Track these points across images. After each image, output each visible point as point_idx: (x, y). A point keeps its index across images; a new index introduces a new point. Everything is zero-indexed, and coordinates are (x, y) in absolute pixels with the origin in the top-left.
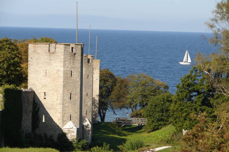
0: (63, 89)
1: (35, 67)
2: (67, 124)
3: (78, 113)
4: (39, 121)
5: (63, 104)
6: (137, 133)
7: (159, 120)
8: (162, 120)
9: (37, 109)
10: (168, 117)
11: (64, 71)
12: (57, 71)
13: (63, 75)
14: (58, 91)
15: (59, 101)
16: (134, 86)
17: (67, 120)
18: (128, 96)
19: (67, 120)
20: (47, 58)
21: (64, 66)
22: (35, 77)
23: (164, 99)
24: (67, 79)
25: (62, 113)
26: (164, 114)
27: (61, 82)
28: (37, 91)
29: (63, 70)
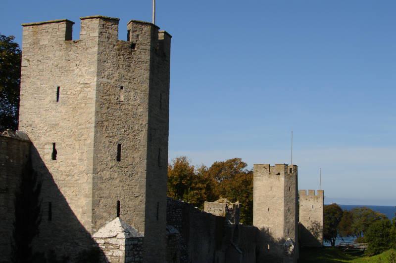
0: (96, 133)
1: (33, 80)
2: (107, 226)
3: (140, 197)
4: (39, 218)
5: (95, 172)
6: (363, 256)
7: (379, 245)
8: (382, 244)
9: (35, 188)
10: (388, 242)
11: (98, 85)
12: (82, 86)
13: (95, 96)
14: (83, 138)
15: (87, 165)
16: (358, 217)
17: (105, 215)
18: (353, 225)
19: (105, 215)
20: (62, 56)
21: (98, 72)
22: (35, 106)
23: (383, 225)
24: (108, 108)
25: (91, 195)
26: (384, 239)
27: (91, 113)
28: (37, 142)
29: (95, 83)
